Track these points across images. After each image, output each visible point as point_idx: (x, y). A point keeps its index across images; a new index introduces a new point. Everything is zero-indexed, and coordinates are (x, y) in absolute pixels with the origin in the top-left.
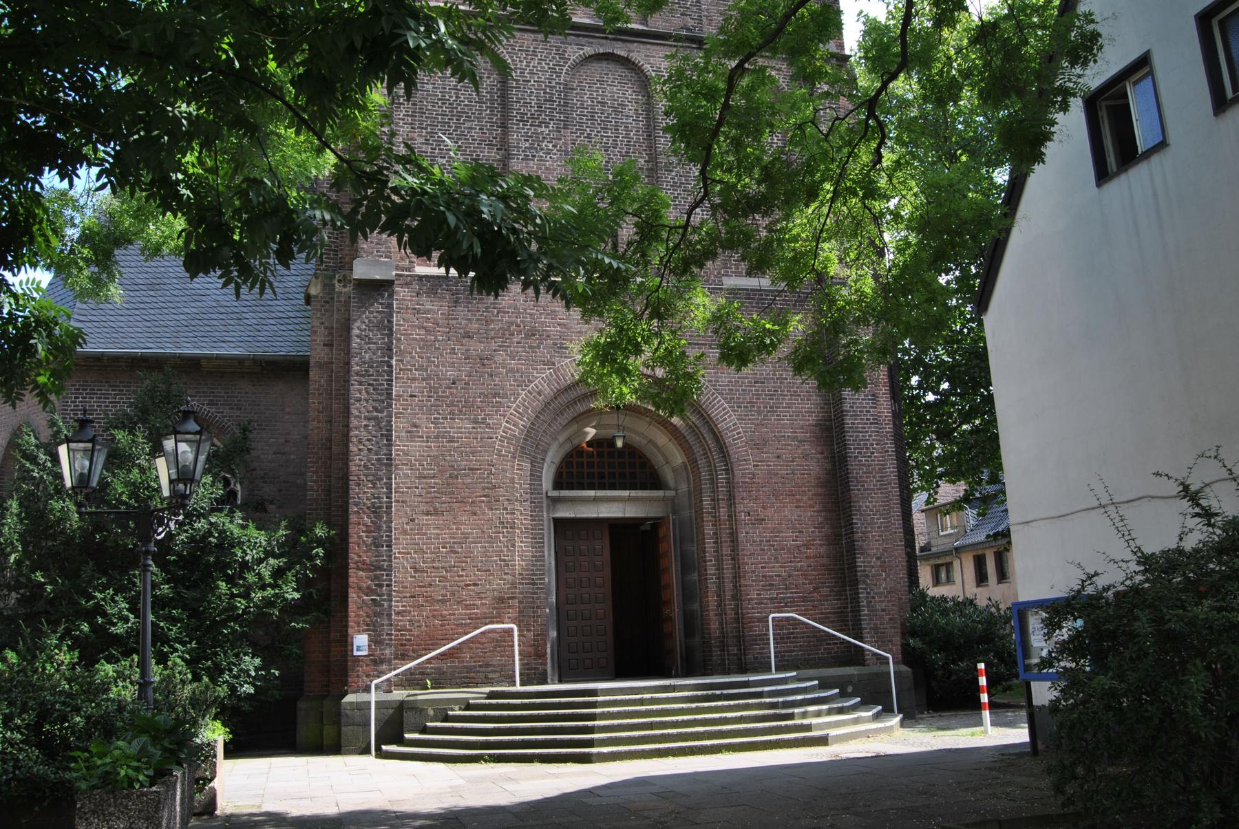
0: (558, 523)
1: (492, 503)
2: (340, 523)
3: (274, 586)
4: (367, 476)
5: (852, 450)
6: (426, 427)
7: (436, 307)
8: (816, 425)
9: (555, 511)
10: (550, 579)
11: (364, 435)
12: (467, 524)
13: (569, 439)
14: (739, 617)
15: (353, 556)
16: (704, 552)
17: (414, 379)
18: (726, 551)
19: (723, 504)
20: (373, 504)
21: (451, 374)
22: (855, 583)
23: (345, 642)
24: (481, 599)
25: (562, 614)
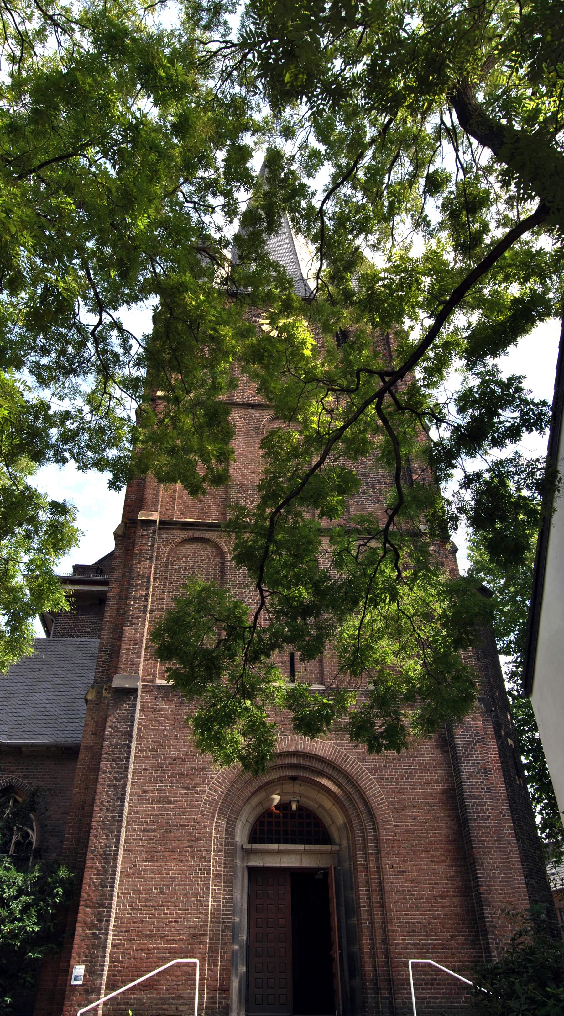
0: (252, 871)
1: (195, 852)
2: (78, 868)
3: (20, 920)
4: (102, 829)
5: (472, 814)
6: (153, 793)
7: (167, 707)
8: (443, 794)
9: (248, 861)
10: (241, 919)
11: (105, 798)
12: (175, 870)
13: (260, 803)
14: (388, 963)
15: (84, 895)
16: (359, 899)
17: (147, 758)
18: (376, 898)
19: (372, 857)
20: (105, 851)
21: (173, 753)
22: (485, 933)
23: (67, 972)
24: (179, 934)
25: (251, 951)
